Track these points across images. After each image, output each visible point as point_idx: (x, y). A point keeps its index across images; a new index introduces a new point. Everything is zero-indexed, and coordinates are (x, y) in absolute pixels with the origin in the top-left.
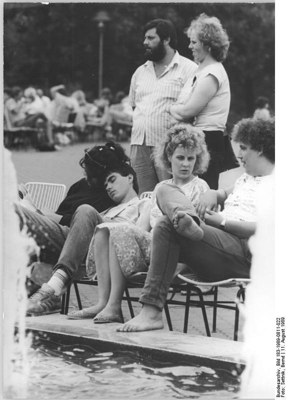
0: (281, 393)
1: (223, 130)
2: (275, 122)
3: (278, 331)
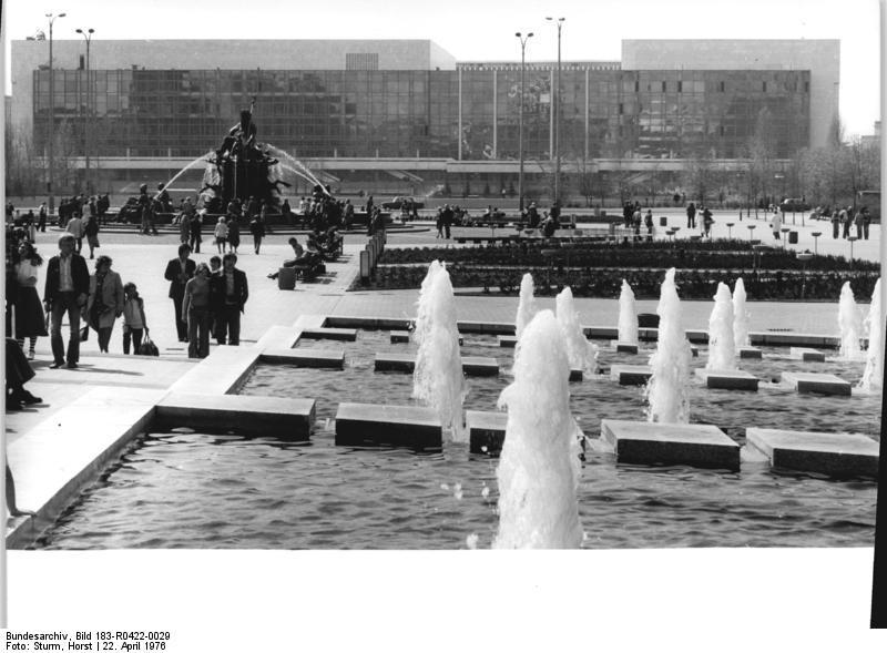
0: (16, 642)
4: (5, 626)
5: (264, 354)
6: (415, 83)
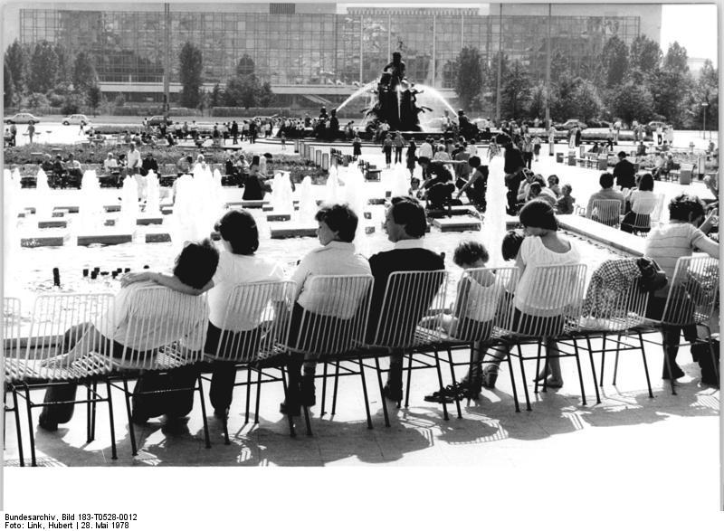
0: (13, 522)
1: (315, 411)
3: (129, 517)
4: (2, 510)
6: (326, 24)
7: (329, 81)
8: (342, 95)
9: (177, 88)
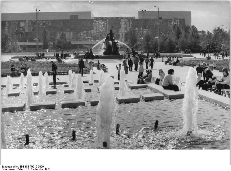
0: (4, 168)
2: (230, 81)
3: (35, 167)
5: (163, 89)
7: (90, 40)
8: (93, 44)
9: (41, 43)
